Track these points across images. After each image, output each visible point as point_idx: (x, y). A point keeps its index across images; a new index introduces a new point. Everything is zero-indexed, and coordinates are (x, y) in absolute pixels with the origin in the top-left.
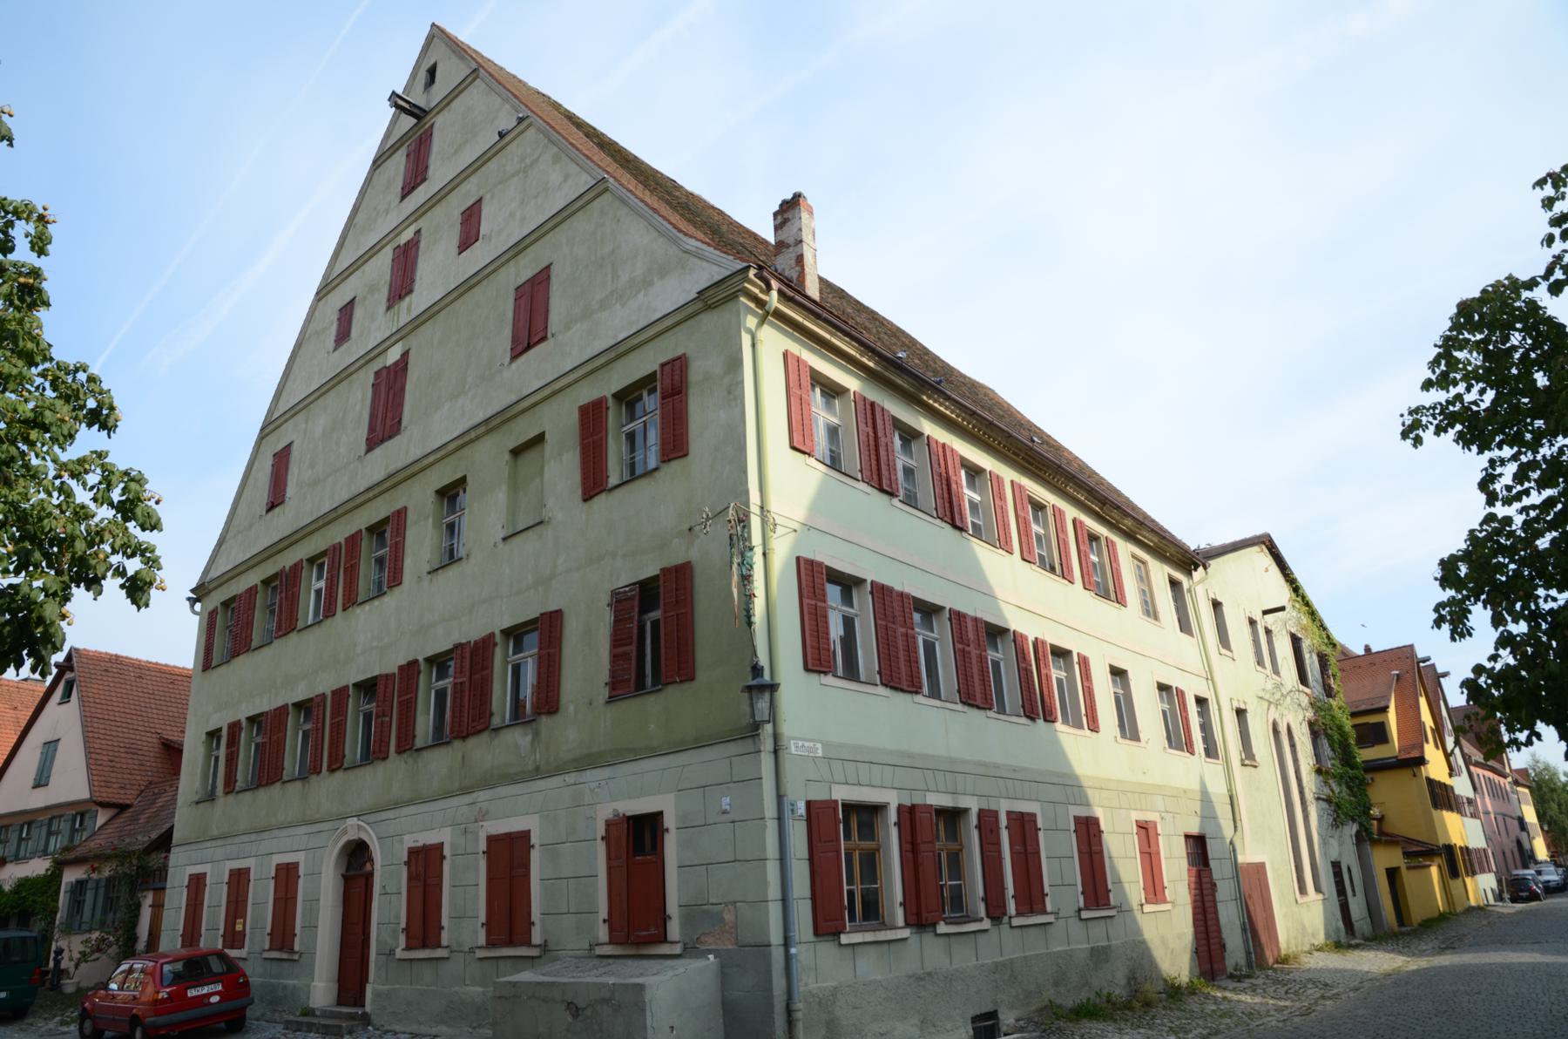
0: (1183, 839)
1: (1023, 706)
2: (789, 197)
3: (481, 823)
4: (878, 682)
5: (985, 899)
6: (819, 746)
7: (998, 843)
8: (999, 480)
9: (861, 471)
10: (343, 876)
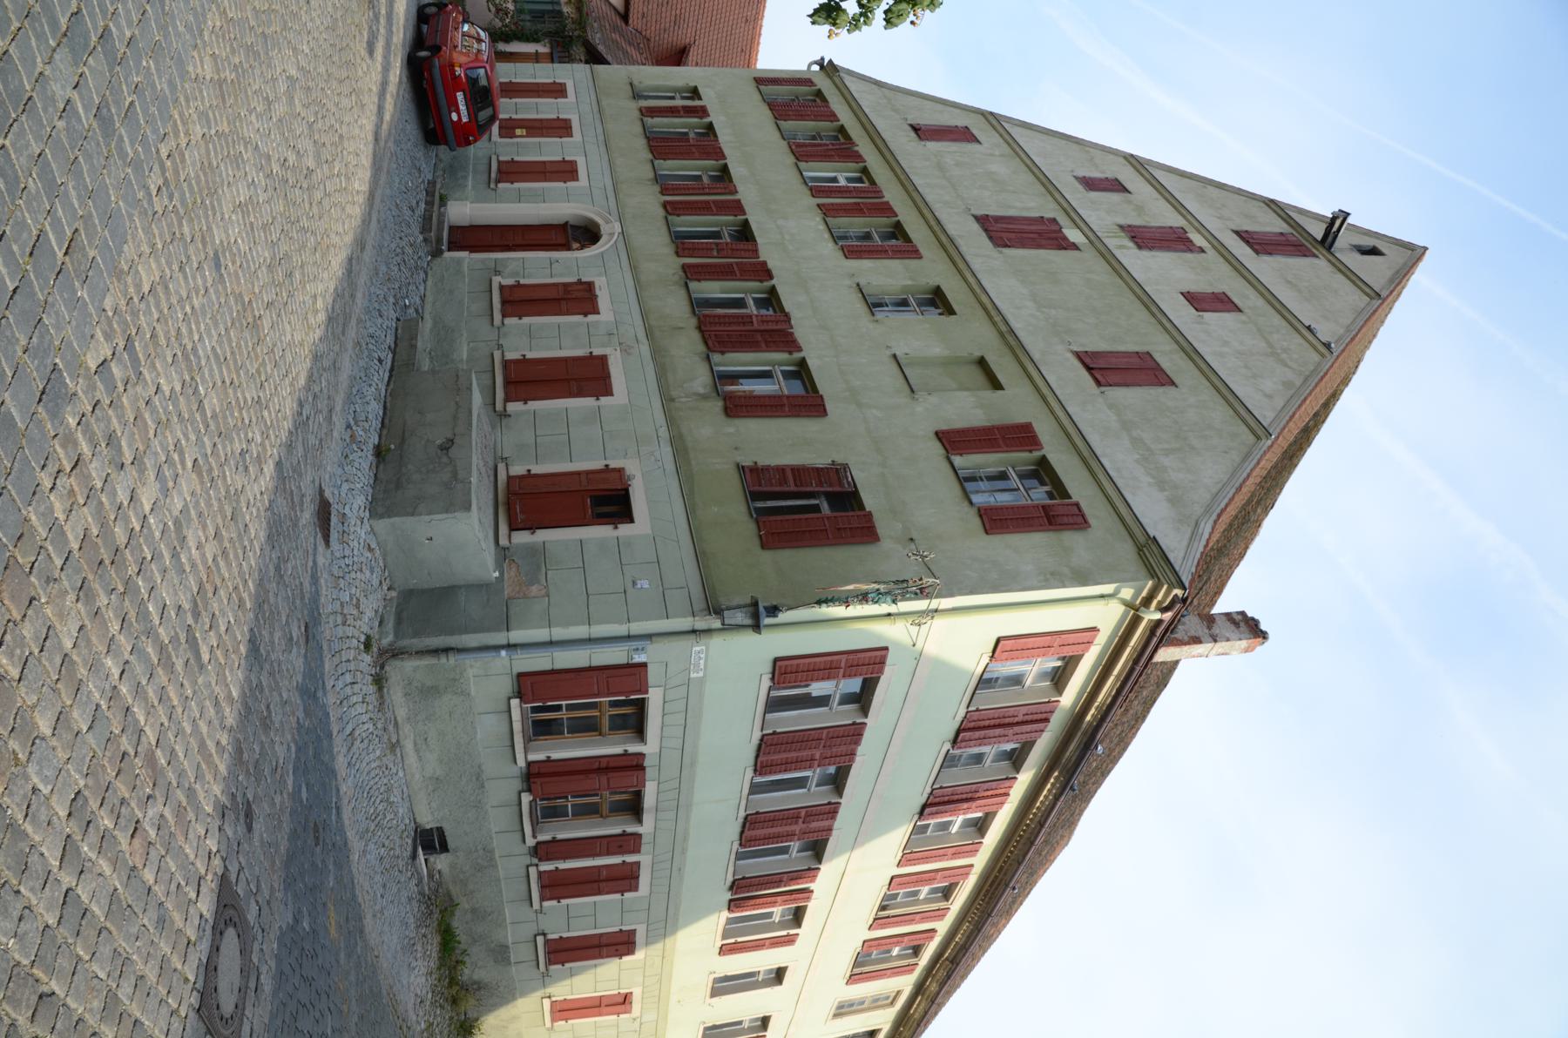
2: (1263, 627)
4: (764, 732)
5: (554, 841)
6: (701, 674)
7: (609, 853)
10: (567, 223)
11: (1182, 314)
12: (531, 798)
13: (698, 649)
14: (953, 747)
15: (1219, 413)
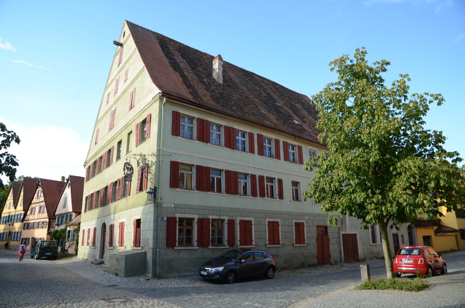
0: (316, 228)
5: (295, 240)
6: (173, 205)
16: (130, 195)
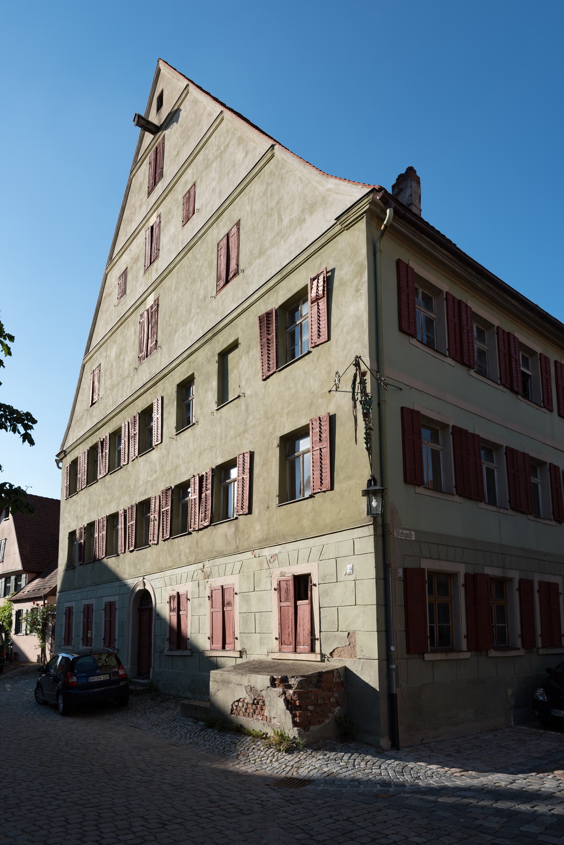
1: (553, 514)
2: (403, 171)
3: (207, 580)
4: (455, 493)
5: (522, 636)
6: (413, 533)
7: (532, 601)
8: (546, 359)
9: (449, 350)
10: (138, 609)
11: (197, 222)
12: (493, 650)
13: (395, 534)
14: (473, 368)
15: (256, 187)
16: (250, 512)
